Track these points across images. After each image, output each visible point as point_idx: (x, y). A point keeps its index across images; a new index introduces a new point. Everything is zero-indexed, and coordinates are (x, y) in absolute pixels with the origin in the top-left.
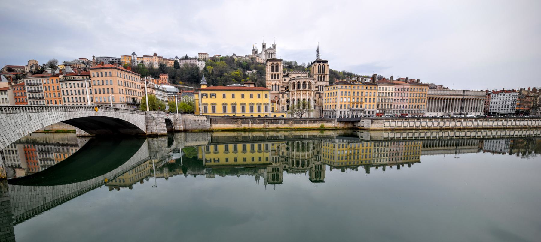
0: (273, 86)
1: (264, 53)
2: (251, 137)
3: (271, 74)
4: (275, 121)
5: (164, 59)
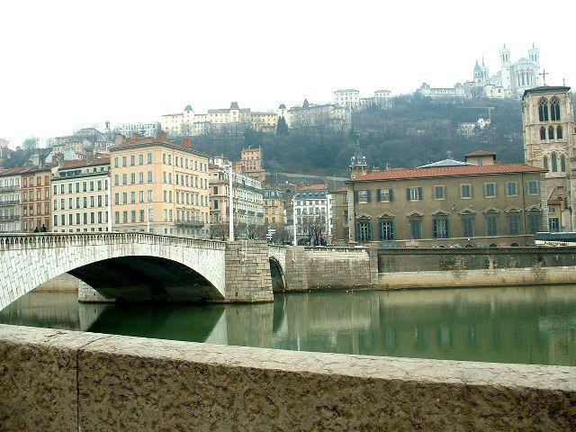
0: (545, 159)
1: (506, 74)
2: (493, 306)
3: (539, 128)
4: (564, 257)
5: (253, 115)
